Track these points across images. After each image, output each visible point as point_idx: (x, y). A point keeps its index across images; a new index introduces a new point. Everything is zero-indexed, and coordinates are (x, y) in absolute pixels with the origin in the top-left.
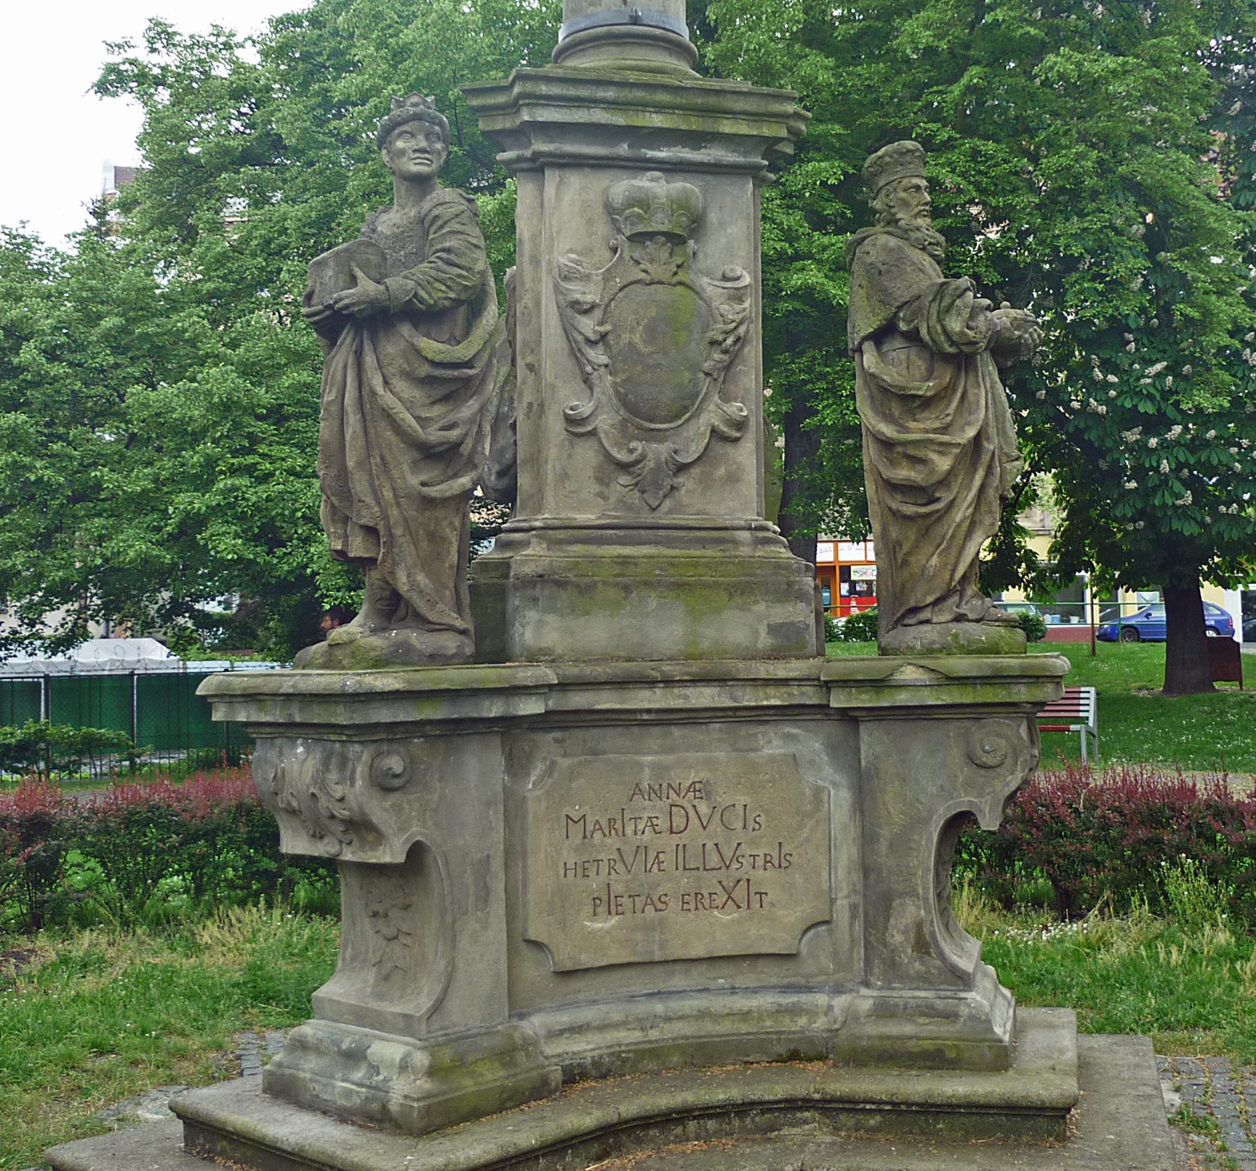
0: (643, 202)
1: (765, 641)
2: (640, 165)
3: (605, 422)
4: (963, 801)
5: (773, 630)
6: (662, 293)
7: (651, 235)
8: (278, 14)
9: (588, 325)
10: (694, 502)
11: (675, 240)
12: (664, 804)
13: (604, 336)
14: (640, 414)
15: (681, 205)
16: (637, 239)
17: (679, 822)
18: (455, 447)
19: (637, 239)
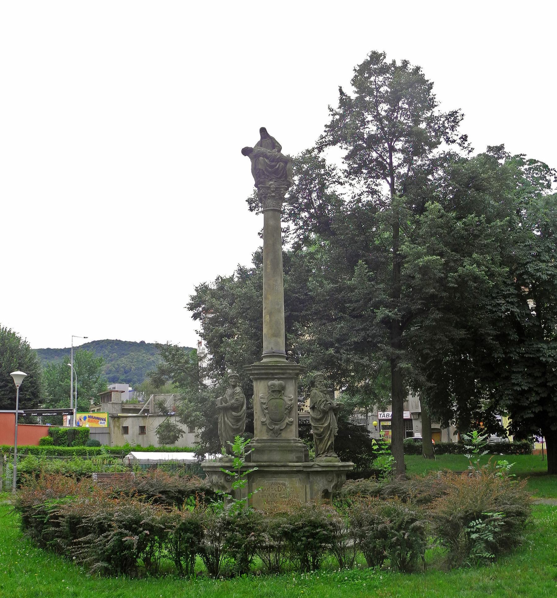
0: (274, 385)
1: (295, 459)
2: (273, 379)
3: (267, 422)
4: (326, 487)
5: (297, 457)
6: (278, 400)
7: (275, 391)
8: (393, 56)
9: (264, 406)
10: (284, 435)
11: (279, 391)
12: (277, 487)
13: (267, 408)
14: (274, 421)
15: (280, 385)
16: (273, 391)
17: (280, 490)
18: (239, 429)
19: (273, 391)
